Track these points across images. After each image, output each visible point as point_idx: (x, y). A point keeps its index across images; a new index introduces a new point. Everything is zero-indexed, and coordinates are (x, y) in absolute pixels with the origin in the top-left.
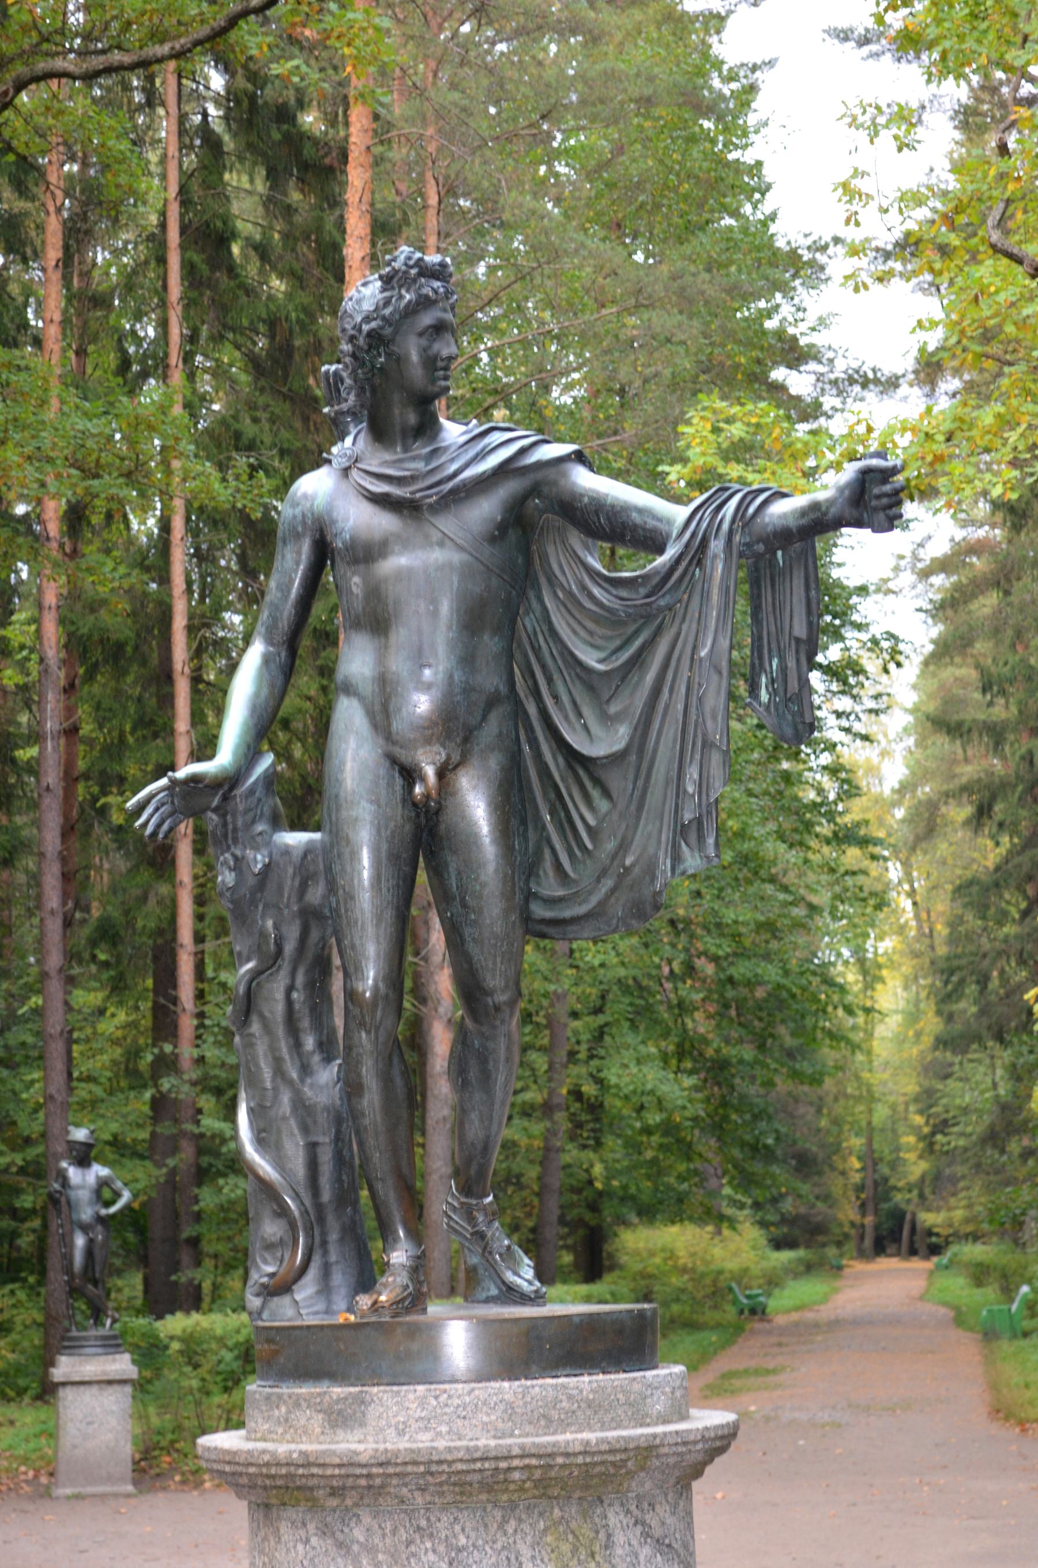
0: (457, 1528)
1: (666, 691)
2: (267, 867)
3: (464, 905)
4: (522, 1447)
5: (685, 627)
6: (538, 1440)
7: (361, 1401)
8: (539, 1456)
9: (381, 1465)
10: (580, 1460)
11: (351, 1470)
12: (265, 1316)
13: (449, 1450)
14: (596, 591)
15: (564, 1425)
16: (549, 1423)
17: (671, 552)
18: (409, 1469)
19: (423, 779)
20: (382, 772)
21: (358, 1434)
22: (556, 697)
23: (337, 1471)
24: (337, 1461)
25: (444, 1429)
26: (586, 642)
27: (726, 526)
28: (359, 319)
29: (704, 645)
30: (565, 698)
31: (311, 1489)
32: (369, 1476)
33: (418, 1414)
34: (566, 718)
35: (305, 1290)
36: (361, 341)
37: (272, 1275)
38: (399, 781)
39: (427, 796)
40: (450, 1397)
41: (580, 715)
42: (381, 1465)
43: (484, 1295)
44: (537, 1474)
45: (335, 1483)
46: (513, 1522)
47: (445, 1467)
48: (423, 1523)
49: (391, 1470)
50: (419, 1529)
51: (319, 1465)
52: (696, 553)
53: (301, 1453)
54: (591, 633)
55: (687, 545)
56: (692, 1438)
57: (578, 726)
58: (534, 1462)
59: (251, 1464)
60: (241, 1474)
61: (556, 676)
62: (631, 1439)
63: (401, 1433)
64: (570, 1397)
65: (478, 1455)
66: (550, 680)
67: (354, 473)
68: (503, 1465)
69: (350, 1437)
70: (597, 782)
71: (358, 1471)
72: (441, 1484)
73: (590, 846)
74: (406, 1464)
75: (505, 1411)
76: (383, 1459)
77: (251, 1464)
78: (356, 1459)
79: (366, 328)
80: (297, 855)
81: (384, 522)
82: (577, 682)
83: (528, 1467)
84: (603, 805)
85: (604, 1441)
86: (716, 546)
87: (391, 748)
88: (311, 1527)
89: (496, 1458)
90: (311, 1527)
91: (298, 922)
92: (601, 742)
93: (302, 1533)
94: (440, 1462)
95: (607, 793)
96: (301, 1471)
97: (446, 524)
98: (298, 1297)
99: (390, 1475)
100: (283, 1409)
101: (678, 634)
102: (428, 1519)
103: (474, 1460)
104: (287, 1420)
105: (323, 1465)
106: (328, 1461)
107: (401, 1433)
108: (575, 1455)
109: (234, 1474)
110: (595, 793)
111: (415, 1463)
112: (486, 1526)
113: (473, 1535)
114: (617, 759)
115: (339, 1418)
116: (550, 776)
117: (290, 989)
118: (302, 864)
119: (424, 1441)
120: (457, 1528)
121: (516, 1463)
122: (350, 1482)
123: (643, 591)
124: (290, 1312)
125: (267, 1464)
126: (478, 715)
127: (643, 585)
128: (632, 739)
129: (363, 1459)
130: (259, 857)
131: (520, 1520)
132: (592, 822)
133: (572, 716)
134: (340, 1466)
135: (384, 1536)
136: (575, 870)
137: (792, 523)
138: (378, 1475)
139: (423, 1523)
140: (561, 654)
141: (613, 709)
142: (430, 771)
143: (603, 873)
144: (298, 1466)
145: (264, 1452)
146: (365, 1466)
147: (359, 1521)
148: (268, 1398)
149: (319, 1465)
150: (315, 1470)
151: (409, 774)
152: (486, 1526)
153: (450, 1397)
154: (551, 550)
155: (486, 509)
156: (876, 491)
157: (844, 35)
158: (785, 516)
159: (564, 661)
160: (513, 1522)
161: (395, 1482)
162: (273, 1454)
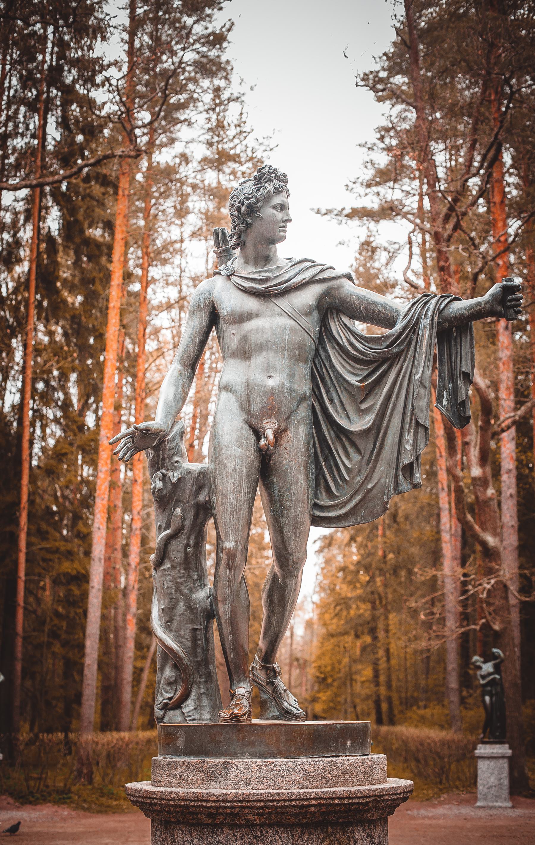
0: (277, 837)
1: (394, 396)
2: (179, 480)
3: (281, 506)
4: (317, 793)
5: (406, 365)
6: (325, 790)
7: (226, 767)
8: (326, 799)
9: (239, 801)
10: (346, 801)
11: (222, 804)
12: (165, 720)
13: (278, 794)
14: (358, 344)
15: (335, 784)
16: (327, 781)
17: (399, 326)
18: (255, 804)
19: (266, 437)
20: (244, 432)
21: (223, 784)
22: (332, 401)
23: (214, 804)
24: (215, 798)
25: (271, 783)
26: (349, 372)
27: (430, 313)
28: (242, 198)
29: (417, 372)
30: (337, 401)
31: (197, 814)
32: (232, 807)
33: (257, 774)
34: (337, 411)
35: (189, 707)
36: (243, 209)
37: (170, 699)
38: (252, 437)
39: (268, 446)
40: (275, 766)
41: (344, 409)
42: (239, 801)
43: (271, 715)
44: (323, 809)
45: (212, 810)
46: (307, 834)
47: (275, 804)
48: (259, 833)
49: (245, 804)
50: (256, 836)
51: (204, 801)
52: (413, 327)
53: (194, 793)
54: (353, 367)
55: (409, 322)
56: (399, 791)
57: (343, 415)
58: (323, 802)
59: (163, 799)
60: (155, 804)
61: (332, 389)
62: (371, 791)
63: (247, 785)
64: (338, 768)
65: (293, 797)
66: (328, 392)
67: (233, 278)
68: (306, 803)
69: (218, 786)
70: (353, 444)
71: (226, 804)
72: (270, 813)
73: (348, 478)
74: (254, 801)
75: (304, 774)
76: (241, 798)
77: (163, 799)
78: (226, 798)
79: (246, 202)
80: (194, 476)
81: (251, 304)
82: (344, 392)
83: (320, 805)
84: (356, 458)
85: (359, 791)
86: (425, 323)
87: (250, 419)
88: (194, 834)
89: (303, 799)
90: (194, 834)
91: (193, 510)
92: (358, 424)
93: (189, 837)
94: (272, 801)
95: (358, 450)
96: (193, 804)
97: (284, 303)
98: (184, 711)
99: (244, 807)
100: (179, 770)
101: (401, 368)
102: (261, 832)
103: (291, 800)
104: (181, 776)
105: (207, 801)
106: (209, 798)
107: (247, 785)
108: (344, 798)
109: (151, 804)
110: (351, 451)
111: (258, 801)
112: (293, 836)
113: (286, 840)
114: (366, 432)
115: (212, 776)
116: (326, 441)
117: (187, 545)
118: (197, 479)
119: (261, 790)
120: (277, 837)
121: (313, 802)
122: (220, 811)
123: (385, 344)
124: (179, 719)
125: (174, 800)
126: (295, 404)
127: (384, 341)
128: (373, 424)
129: (230, 798)
130: (175, 474)
131: (311, 833)
132: (349, 465)
133: (340, 410)
134: (215, 801)
135: (236, 840)
136: (338, 490)
137: (464, 312)
138: (238, 807)
139: (259, 833)
140: (336, 378)
141: (363, 406)
142: (270, 434)
143: (356, 493)
144: (192, 801)
145: (171, 793)
146: (231, 801)
147: (222, 832)
148: (170, 764)
149: (204, 801)
150: (202, 803)
151: (258, 434)
152: (293, 836)
153: (275, 766)
154: (332, 324)
155: (308, 297)
156: (509, 298)
157: (318, 212)
158: (461, 309)
159: (338, 381)
160: (307, 834)
161: (246, 811)
162: (178, 794)
